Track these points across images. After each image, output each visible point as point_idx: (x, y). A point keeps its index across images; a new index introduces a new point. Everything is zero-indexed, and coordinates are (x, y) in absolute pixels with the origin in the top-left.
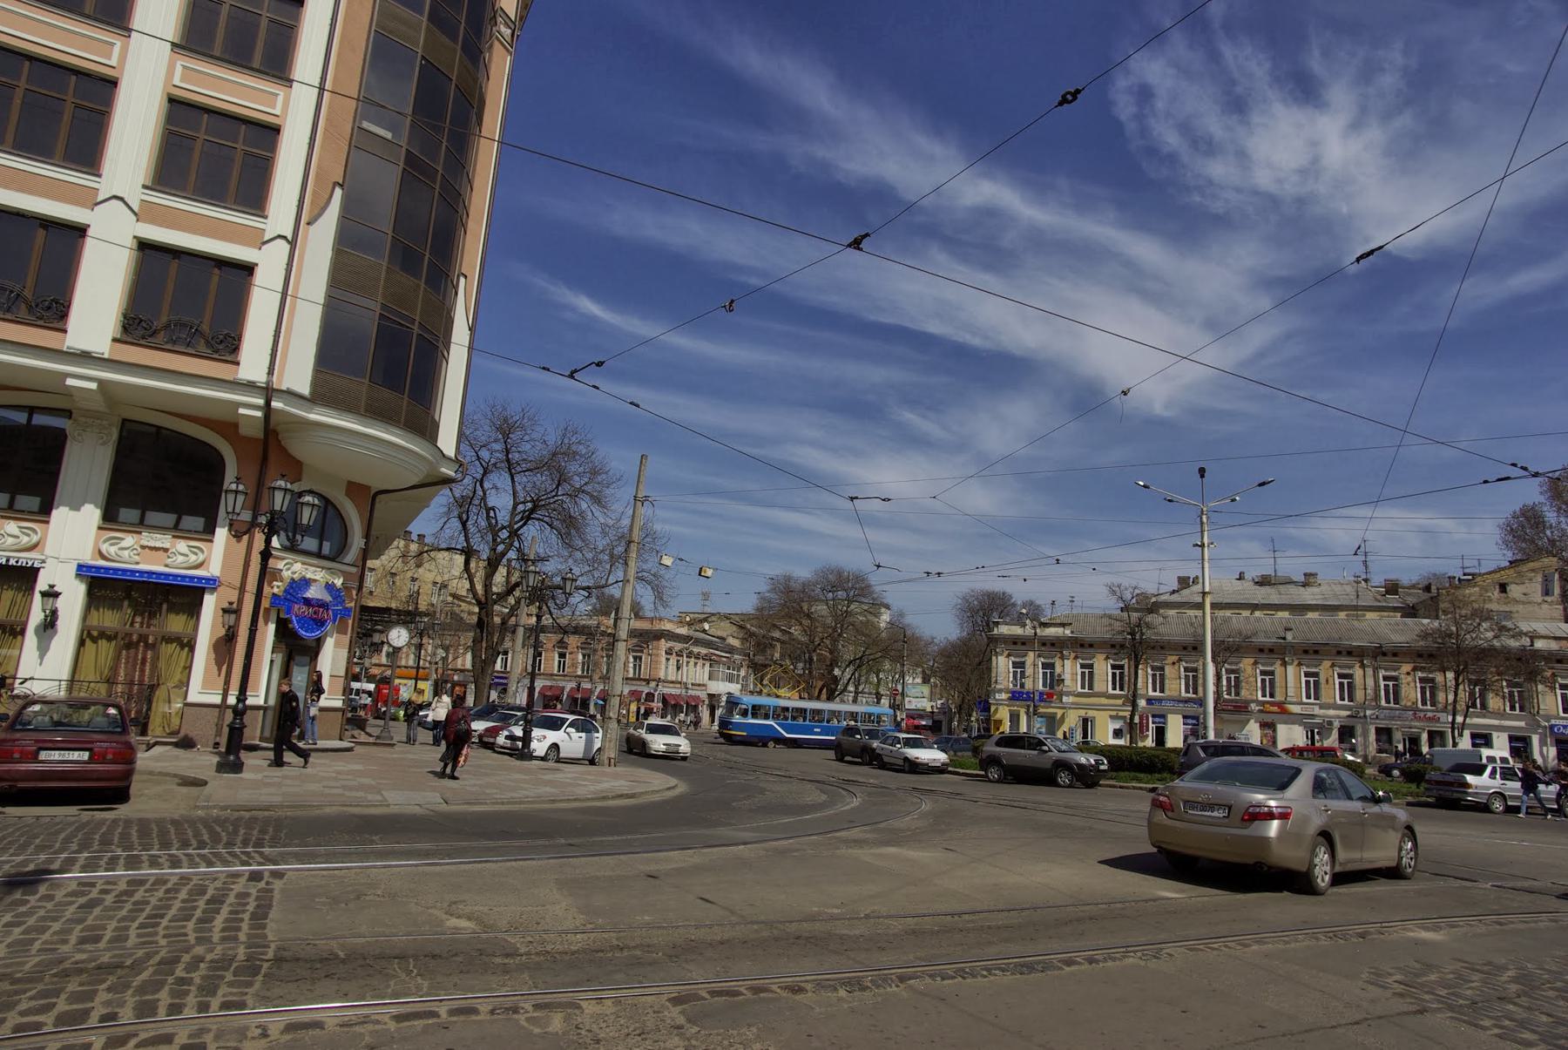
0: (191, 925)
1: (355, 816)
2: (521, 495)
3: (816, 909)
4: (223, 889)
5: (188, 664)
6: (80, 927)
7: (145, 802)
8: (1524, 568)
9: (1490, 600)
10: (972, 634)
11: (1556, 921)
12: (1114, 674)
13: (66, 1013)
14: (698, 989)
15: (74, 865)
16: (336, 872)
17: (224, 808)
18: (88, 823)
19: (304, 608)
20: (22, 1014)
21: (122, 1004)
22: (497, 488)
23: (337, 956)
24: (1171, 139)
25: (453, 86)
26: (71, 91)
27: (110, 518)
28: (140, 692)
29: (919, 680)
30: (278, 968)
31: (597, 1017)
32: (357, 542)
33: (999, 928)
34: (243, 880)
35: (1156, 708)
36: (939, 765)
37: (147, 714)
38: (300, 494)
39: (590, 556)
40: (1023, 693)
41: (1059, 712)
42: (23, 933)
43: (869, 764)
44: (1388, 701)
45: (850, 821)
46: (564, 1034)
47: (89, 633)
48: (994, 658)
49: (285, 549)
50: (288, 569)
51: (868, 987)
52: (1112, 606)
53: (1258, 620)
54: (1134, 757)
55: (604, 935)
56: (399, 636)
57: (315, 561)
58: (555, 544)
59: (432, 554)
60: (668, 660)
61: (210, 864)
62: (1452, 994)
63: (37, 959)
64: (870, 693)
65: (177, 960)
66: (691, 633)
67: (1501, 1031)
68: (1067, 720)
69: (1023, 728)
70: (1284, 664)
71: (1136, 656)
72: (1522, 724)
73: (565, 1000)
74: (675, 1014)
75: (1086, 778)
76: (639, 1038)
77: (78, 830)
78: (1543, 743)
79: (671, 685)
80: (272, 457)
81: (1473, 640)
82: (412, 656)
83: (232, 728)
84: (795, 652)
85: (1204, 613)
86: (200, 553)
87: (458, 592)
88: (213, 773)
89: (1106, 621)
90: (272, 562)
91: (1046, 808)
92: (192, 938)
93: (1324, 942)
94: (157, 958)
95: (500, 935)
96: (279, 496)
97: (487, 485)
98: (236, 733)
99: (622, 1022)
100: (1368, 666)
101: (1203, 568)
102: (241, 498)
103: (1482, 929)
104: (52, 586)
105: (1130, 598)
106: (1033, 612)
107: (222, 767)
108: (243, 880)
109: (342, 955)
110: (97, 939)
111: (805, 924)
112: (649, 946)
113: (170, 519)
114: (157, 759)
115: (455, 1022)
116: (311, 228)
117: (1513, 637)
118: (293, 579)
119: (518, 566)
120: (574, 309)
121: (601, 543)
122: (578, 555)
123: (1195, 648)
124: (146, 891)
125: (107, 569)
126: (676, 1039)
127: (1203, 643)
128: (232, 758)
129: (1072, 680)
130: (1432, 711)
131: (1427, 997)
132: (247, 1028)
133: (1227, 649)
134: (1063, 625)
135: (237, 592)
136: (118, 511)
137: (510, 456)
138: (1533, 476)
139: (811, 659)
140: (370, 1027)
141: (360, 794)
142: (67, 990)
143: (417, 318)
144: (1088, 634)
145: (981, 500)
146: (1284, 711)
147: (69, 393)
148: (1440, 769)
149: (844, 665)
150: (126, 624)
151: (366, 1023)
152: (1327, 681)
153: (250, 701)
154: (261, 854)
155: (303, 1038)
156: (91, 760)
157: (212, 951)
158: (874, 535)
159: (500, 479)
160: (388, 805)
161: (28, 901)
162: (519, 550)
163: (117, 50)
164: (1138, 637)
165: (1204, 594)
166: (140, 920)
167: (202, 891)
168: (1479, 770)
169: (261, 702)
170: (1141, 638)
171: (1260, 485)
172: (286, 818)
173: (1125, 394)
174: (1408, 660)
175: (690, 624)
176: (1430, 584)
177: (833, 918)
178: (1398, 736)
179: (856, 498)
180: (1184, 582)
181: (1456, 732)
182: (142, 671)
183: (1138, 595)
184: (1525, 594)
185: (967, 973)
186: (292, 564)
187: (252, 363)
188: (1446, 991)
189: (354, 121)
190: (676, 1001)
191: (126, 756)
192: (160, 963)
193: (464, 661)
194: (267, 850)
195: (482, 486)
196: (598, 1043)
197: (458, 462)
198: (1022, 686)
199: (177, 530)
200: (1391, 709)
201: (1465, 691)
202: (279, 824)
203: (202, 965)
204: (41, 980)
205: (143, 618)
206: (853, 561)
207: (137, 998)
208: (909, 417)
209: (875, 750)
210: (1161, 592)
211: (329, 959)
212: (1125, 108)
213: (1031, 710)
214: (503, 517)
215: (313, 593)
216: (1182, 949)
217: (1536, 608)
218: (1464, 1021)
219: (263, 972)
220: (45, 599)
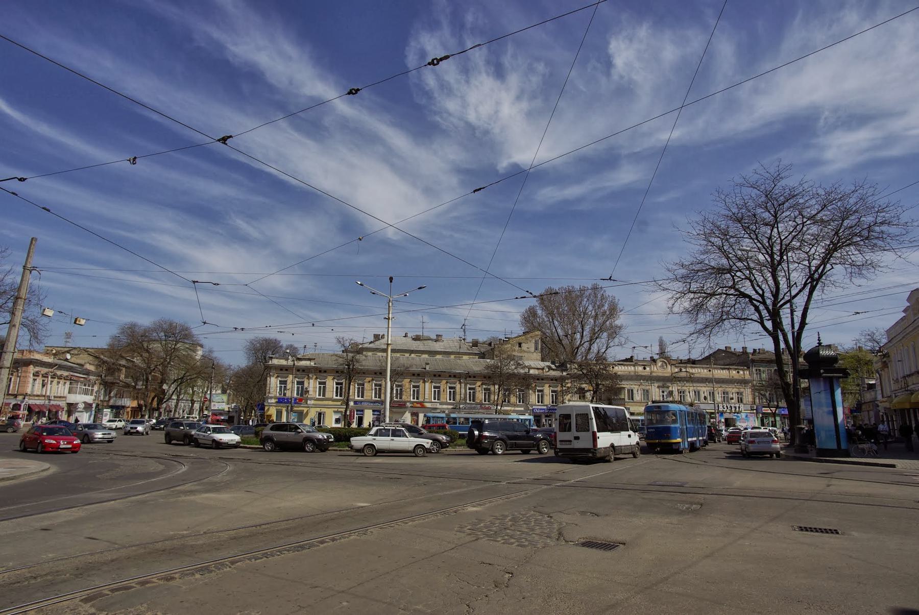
3: (172, 533)
8: (528, 336)
9: (515, 351)
10: (255, 364)
12: (337, 388)
14: (102, 590)
29: (219, 392)
36: (235, 443)
40: (284, 399)
41: (305, 410)
43: (189, 444)
44: (470, 400)
45: (184, 479)
48: (268, 378)
51: (213, 570)
52: (339, 350)
53: (413, 359)
54: (347, 434)
55: (16, 572)
60: (35, 380)
62: (488, 530)
64: (187, 400)
66: (57, 361)
69: (284, 420)
70: (424, 382)
71: (350, 377)
72: (522, 409)
75: (322, 447)
79: (36, 398)
84: (135, 373)
89: (334, 358)
105: (348, 345)
106: (293, 352)
111: (167, 542)
112: (57, 572)
117: (522, 368)
123: (381, 373)
127: (386, 370)
131: (479, 533)
133: (397, 374)
134: (310, 359)
139: (147, 379)
144: (323, 365)
145: (278, 281)
146: (423, 407)
149: (170, 383)
152: (444, 391)
158: (205, 298)
164: (351, 367)
175: (55, 355)
177: (183, 536)
180: (377, 337)
183: (352, 344)
184: (528, 348)
185: (269, 555)
190: (86, 600)
198: (285, 394)
200: (471, 404)
208: (241, 223)
209: (193, 435)
213: (289, 408)
216: (377, 529)
218: (492, 540)
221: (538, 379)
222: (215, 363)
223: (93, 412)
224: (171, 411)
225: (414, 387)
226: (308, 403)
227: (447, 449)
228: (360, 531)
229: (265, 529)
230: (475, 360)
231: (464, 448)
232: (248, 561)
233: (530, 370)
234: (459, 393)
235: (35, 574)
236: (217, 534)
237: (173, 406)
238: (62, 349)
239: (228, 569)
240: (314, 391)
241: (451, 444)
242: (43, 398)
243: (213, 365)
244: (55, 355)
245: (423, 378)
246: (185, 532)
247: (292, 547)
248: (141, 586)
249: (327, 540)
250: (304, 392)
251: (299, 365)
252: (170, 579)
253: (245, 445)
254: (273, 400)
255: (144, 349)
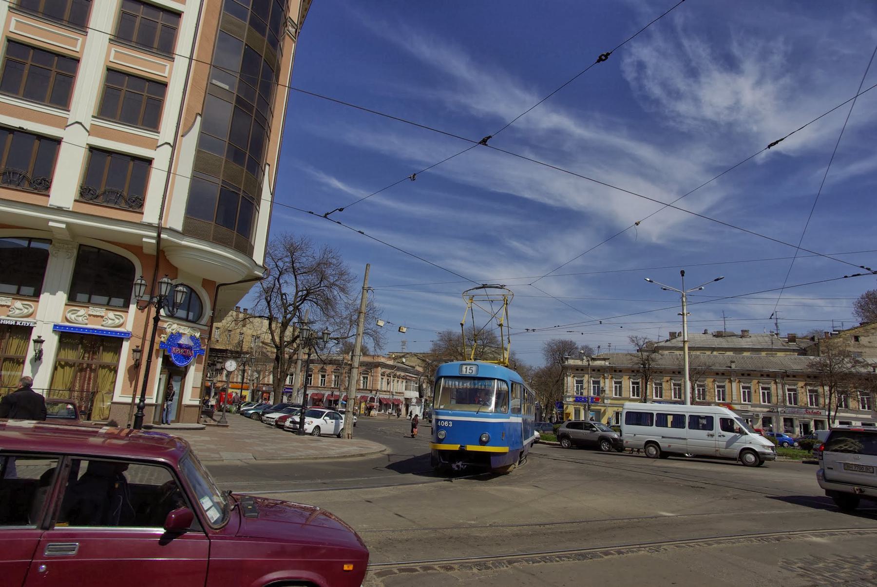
3: (462, 521)
8: (869, 327)
12: (633, 387)
40: (582, 398)
41: (603, 409)
48: (565, 378)
52: (632, 348)
53: (715, 356)
60: (382, 379)
66: (395, 364)
69: (582, 418)
70: (731, 382)
72: (870, 417)
79: (384, 393)
89: (629, 357)
105: (642, 344)
106: (588, 353)
111: (455, 530)
117: (863, 366)
123: (679, 373)
127: (684, 369)
131: (818, 577)
133: (698, 373)
134: (604, 359)
144: (617, 364)
164: (647, 366)
177: (471, 526)
180: (673, 335)
183: (647, 342)
185: (548, 559)
198: (582, 394)
213: (587, 407)
216: (672, 546)
222: (517, 364)
223: (423, 406)
225: (718, 387)
228: (652, 546)
229: (549, 529)
230: (793, 357)
231: (786, 458)
234: (776, 395)
238: (400, 354)
240: (610, 390)
242: (389, 393)
243: (515, 366)
244: (395, 359)
245: (729, 377)
246: (473, 522)
248: (424, 571)
249: (612, 551)
250: (600, 392)
252: (449, 568)
253: (544, 441)
254: (571, 399)
255: (459, 352)
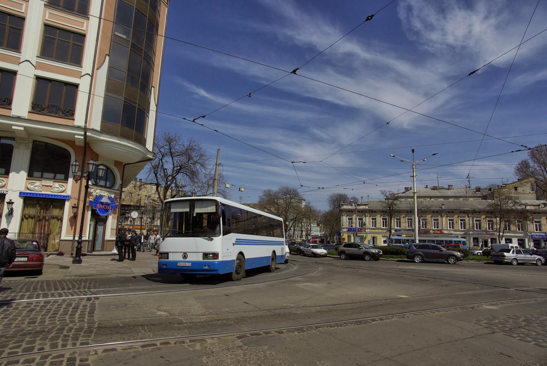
0: (67, 316)
1: (121, 277)
2: (176, 164)
4: (78, 304)
5: (61, 226)
6: (29, 318)
7: (48, 274)
8: (523, 182)
9: (512, 193)
11: (536, 301)
13: (26, 348)
15: (25, 297)
16: (117, 297)
17: (76, 276)
18: (28, 282)
19: (101, 206)
20: (11, 349)
21: (45, 344)
22: (167, 162)
23: (119, 326)
24: (417, 24)
25: (147, 19)
26: (8, 22)
27: (30, 175)
28: (44, 236)
29: (316, 225)
30: (100, 330)
31: (212, 344)
32: (119, 182)
33: (349, 309)
34: (85, 301)
35: (398, 233)
36: (324, 254)
37: (47, 244)
38: (98, 166)
39: (200, 185)
40: (352, 229)
41: (365, 235)
42: (8, 321)
43: (300, 254)
44: (477, 228)
46: (201, 350)
47: (25, 216)
48: (342, 217)
49: (93, 185)
50: (95, 192)
51: (305, 331)
52: (383, 198)
53: (433, 202)
56: (135, 214)
57: (104, 189)
58: (188, 181)
59: (145, 186)
61: (73, 295)
63: (14, 330)
64: (299, 230)
65: (63, 329)
67: (520, 338)
68: (367, 238)
70: (442, 217)
71: (391, 215)
72: (522, 235)
73: (201, 338)
74: (239, 342)
75: (375, 257)
76: (227, 351)
77: (25, 285)
78: (529, 241)
80: (88, 152)
81: (506, 206)
82: (139, 222)
83: (77, 248)
85: (414, 200)
86: (63, 187)
87: (155, 199)
88: (71, 264)
89: (380, 203)
90: (89, 190)
91: (361, 268)
92: (68, 321)
93: (460, 311)
94: (56, 329)
95: (177, 317)
96: (91, 166)
97: (163, 161)
98: (79, 250)
99: (221, 345)
100: (470, 217)
101: (414, 184)
102: (77, 167)
103: (512, 304)
104: (11, 200)
106: (355, 201)
107: (74, 262)
108: (85, 301)
109: (121, 325)
110: (35, 322)
111: (282, 310)
112: (228, 319)
113: (52, 175)
114: (51, 259)
115: (163, 347)
116: (99, 71)
117: (519, 205)
118: (96, 195)
119: (175, 189)
120: (196, 94)
121: (204, 180)
122: (196, 185)
123: (411, 212)
124: (51, 305)
125: (30, 194)
126: (240, 350)
127: (414, 210)
128: (78, 258)
129: (369, 224)
130: (492, 231)
131: (495, 328)
132: (90, 351)
133: (422, 212)
134: (365, 205)
135: (77, 200)
136: (33, 174)
137: (171, 151)
138: (529, 149)
140: (133, 350)
141: (124, 270)
142: (26, 340)
143: (137, 102)
144: (373, 208)
145: (340, 161)
147: (14, 131)
148: (495, 251)
149: (290, 221)
150: (38, 213)
151: (131, 348)
152: (456, 222)
153: (83, 239)
154: (90, 291)
155: (110, 354)
156: (28, 260)
157: (76, 325)
158: (300, 174)
159: (168, 159)
160: (134, 273)
161: (9, 310)
162: (175, 183)
163: (24, 6)
165: (414, 193)
166: (49, 315)
167: (70, 305)
168: (508, 251)
169: (87, 239)
170: (392, 209)
171: (433, 155)
172: (98, 279)
173: (388, 124)
174: (484, 214)
176: (491, 188)
177: (291, 308)
178: (480, 240)
179: (294, 162)
180: (407, 189)
181: (500, 238)
182: (44, 229)
184: (523, 191)
185: (339, 325)
186: (96, 190)
187: (79, 119)
188: (501, 326)
189: (112, 32)
190: (239, 338)
191: (41, 259)
192: (57, 330)
193: (157, 223)
194: (92, 290)
195: (162, 161)
196: (213, 353)
197: (153, 153)
198: (352, 226)
199: (54, 179)
201: (503, 224)
202: (96, 281)
203: (72, 330)
204: (16, 337)
205: (44, 211)
206: (292, 184)
207: (51, 342)
208: (316, 131)
209: (301, 249)
210: (399, 193)
211: (117, 327)
212: (402, 14)
213: (355, 234)
214: (170, 172)
215: (104, 200)
217: (527, 195)
218: (507, 335)
219: (94, 332)
220: (9, 204)
221: (535, 213)
224: (291, 236)
226: (366, 231)
227: (462, 262)
230: (478, 201)
231: (475, 261)
232: (326, 328)
233: (527, 206)
234: (468, 224)
235: (219, 318)
236: (310, 308)
237: (292, 234)
239: (314, 331)
241: (465, 258)
243: (311, 210)
246: (292, 305)
247: (354, 321)
248: (266, 334)
249: (377, 319)
250: (363, 225)
251: (359, 208)
253: (330, 256)
